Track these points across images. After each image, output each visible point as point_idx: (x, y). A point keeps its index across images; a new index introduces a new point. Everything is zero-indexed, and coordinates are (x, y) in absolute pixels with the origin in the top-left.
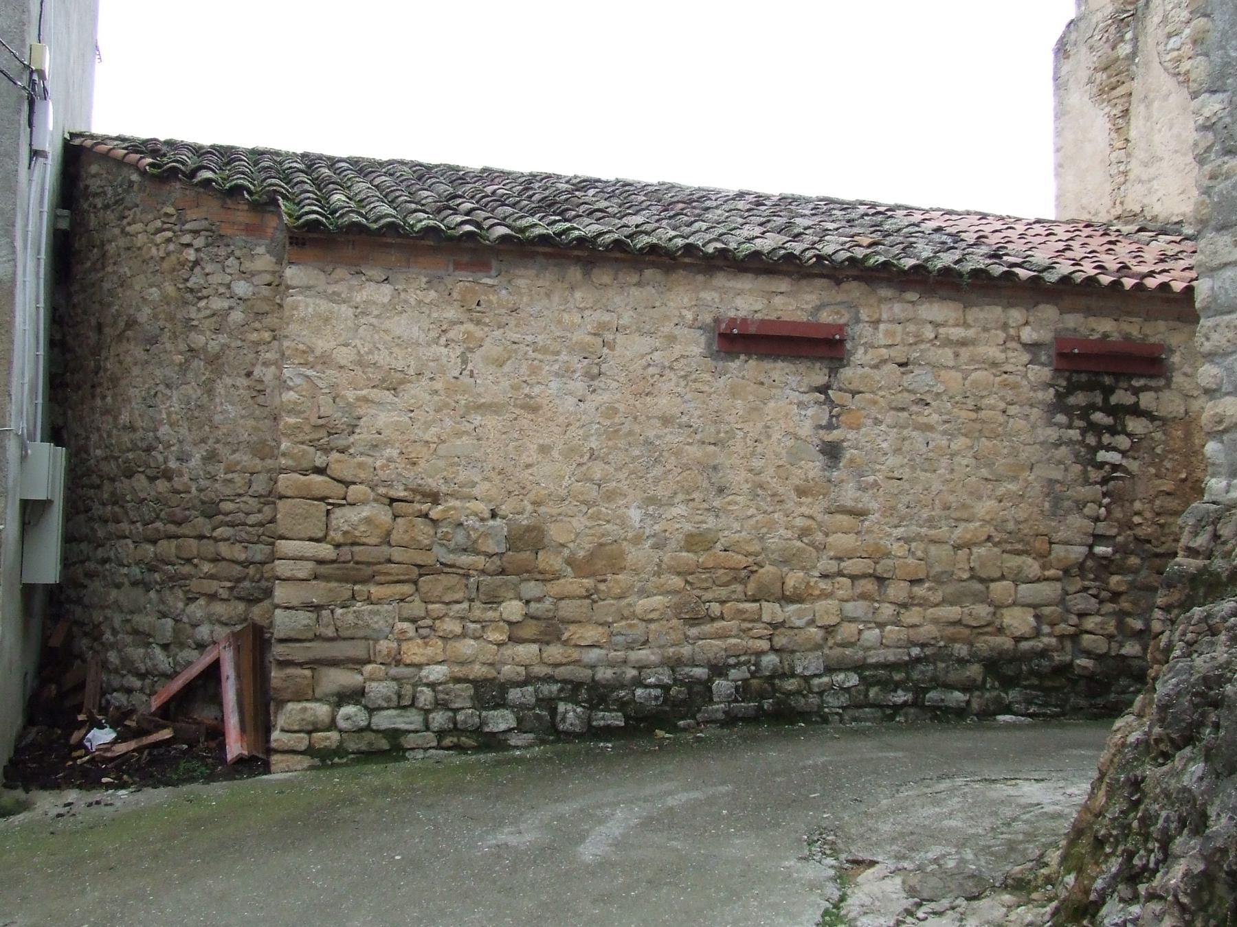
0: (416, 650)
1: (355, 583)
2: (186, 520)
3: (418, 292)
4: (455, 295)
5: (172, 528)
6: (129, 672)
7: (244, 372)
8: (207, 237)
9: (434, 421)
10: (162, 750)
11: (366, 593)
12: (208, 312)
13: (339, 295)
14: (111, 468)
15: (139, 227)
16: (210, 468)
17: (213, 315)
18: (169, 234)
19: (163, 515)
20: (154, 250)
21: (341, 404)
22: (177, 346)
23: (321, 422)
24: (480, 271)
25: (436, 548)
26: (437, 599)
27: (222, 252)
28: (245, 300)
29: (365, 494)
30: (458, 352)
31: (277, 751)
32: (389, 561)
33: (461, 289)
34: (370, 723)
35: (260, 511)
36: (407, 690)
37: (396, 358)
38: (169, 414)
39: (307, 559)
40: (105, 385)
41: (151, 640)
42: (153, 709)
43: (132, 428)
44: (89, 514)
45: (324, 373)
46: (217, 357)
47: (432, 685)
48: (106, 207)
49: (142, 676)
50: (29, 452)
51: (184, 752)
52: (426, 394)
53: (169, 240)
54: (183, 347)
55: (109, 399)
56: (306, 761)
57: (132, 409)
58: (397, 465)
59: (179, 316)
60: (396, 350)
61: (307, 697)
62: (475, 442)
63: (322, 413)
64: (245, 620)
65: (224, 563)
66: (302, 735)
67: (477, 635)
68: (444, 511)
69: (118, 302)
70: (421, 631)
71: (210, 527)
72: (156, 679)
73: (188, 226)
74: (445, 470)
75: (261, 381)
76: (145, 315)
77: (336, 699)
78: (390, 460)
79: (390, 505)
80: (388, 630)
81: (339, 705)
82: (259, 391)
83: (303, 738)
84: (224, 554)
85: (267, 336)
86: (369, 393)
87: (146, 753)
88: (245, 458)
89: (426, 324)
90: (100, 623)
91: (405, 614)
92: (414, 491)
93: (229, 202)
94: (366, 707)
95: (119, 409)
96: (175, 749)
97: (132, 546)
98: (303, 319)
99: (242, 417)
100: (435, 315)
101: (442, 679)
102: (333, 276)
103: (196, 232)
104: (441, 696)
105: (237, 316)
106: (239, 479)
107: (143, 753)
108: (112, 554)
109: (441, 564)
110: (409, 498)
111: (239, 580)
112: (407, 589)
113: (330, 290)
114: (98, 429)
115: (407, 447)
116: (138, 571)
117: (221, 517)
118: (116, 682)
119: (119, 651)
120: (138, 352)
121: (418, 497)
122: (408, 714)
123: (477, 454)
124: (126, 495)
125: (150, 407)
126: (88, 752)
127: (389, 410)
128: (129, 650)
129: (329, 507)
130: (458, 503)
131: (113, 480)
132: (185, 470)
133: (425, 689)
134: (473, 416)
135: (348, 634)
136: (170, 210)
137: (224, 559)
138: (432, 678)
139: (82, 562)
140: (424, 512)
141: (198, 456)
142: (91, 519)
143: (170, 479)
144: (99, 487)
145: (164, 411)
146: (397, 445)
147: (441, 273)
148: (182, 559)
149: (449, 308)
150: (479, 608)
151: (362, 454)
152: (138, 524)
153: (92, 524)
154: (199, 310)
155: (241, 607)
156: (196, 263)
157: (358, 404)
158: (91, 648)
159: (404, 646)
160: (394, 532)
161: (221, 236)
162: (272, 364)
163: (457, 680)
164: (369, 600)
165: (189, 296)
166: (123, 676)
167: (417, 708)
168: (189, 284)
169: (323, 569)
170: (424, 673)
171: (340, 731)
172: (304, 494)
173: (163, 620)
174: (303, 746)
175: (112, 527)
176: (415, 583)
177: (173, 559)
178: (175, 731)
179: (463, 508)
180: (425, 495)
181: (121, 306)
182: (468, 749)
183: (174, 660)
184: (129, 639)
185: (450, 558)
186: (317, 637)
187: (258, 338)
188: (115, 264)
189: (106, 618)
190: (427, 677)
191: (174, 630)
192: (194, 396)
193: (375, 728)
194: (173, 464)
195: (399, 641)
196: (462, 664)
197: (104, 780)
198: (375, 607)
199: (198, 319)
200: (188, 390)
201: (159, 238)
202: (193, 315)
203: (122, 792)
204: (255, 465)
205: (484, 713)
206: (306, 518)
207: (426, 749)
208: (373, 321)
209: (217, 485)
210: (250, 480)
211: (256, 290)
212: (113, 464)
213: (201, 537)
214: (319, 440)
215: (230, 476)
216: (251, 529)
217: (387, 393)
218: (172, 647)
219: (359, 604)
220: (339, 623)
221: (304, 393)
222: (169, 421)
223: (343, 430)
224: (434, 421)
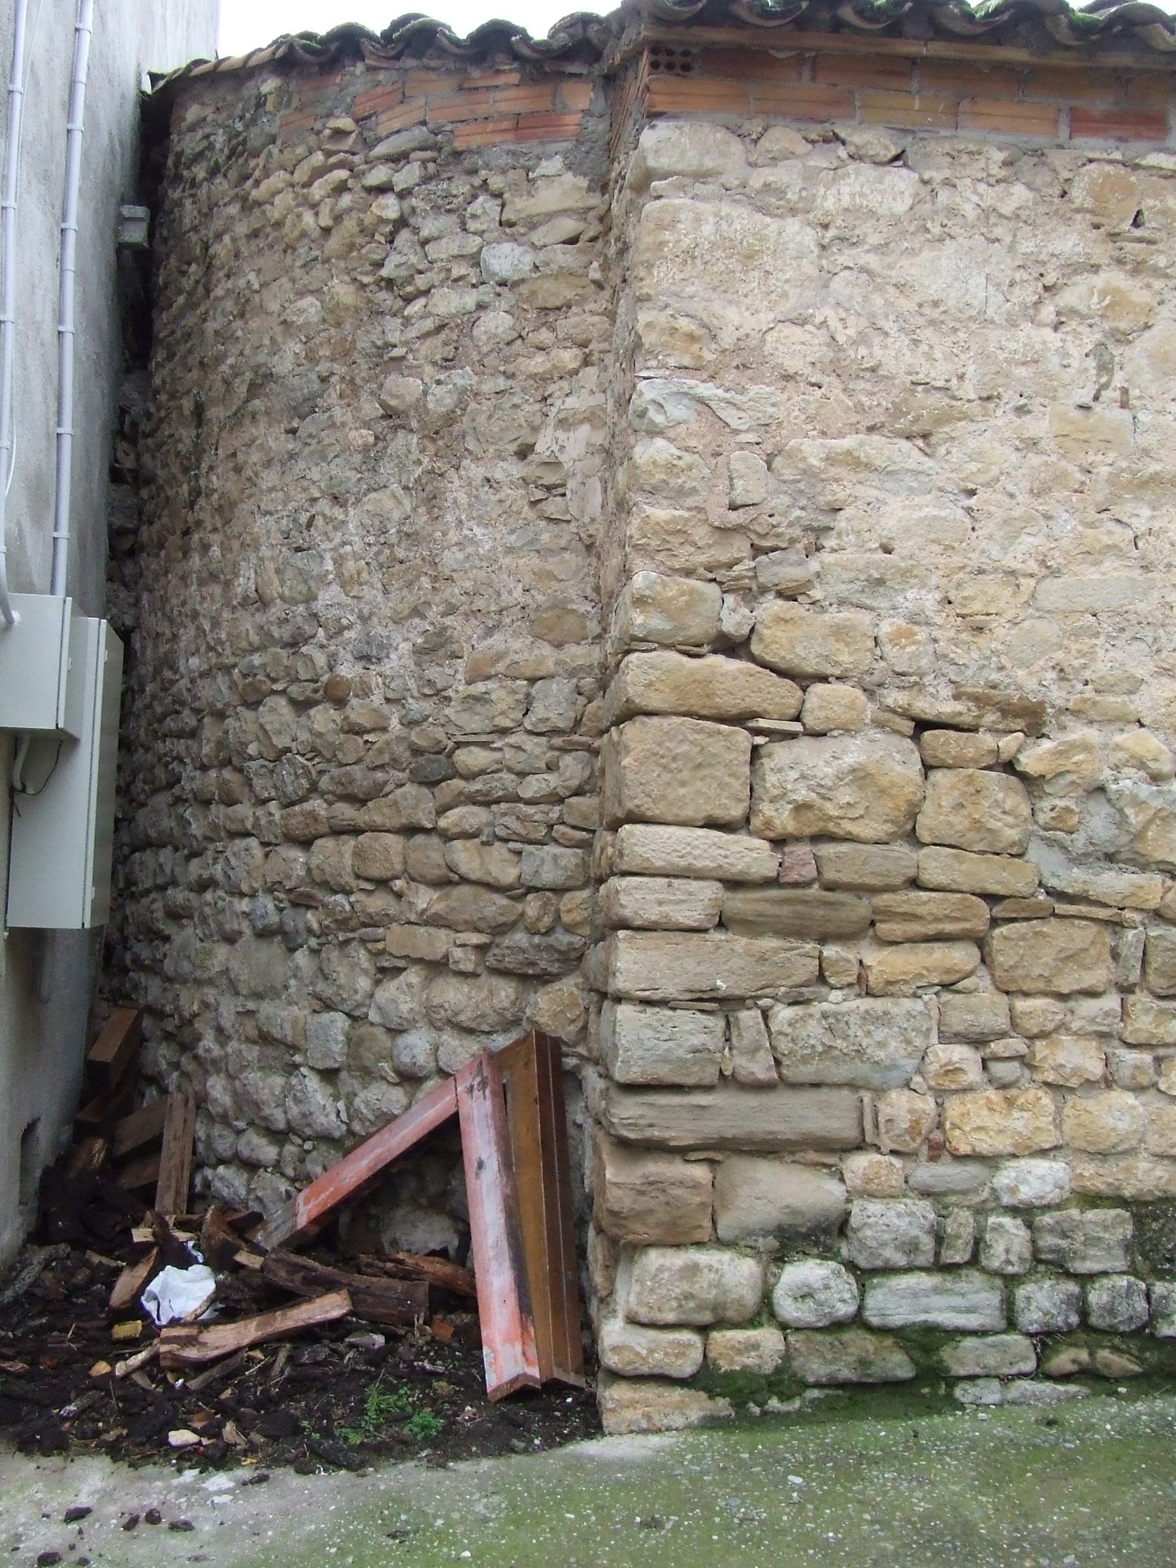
0: (983, 1117)
1: (823, 940)
2: (377, 792)
3: (982, 187)
4: (1078, 195)
5: (346, 812)
6: (251, 1124)
7: (513, 447)
8: (424, 163)
9: (1028, 520)
10: (323, 1353)
11: (855, 969)
12: (429, 324)
13: (780, 193)
14: (217, 691)
15: (278, 179)
16: (433, 673)
17: (440, 328)
18: (342, 174)
19: (324, 783)
20: (308, 218)
21: (788, 474)
22: (358, 409)
23: (735, 517)
24: (1139, 136)
25: (1036, 852)
26: (1041, 985)
27: (461, 187)
28: (516, 284)
29: (851, 707)
30: (1091, 339)
31: (616, 1376)
32: (915, 883)
33: (1093, 181)
34: (861, 1308)
35: (551, 768)
36: (961, 1223)
37: (930, 358)
38: (339, 561)
39: (699, 875)
40: (208, 525)
41: (298, 1058)
42: (302, 1221)
43: (261, 602)
44: (176, 790)
45: (743, 391)
46: (450, 419)
47: (1025, 1212)
48: (214, 172)
49: (279, 1136)
50: (16, 615)
51: (376, 1358)
52: (1008, 451)
53: (341, 188)
54: (371, 409)
55: (216, 551)
56: (697, 1406)
57: (261, 559)
58: (936, 633)
59: (363, 343)
60: (927, 334)
61: (699, 1235)
62: (1136, 574)
63: (740, 497)
64: (516, 1022)
65: (465, 889)
66: (686, 1336)
67: (1144, 1080)
68: (1059, 753)
69: (234, 350)
70: (997, 1068)
71: (431, 805)
72: (308, 1146)
73: (381, 149)
74: (1060, 646)
75: (553, 464)
76: (289, 356)
77: (772, 1242)
78: (916, 618)
79: (916, 737)
80: (910, 1064)
81: (780, 1258)
82: (549, 488)
83: (689, 1345)
84: (464, 869)
85: (569, 358)
86: (861, 444)
87: (282, 1356)
88: (517, 644)
89: (1003, 265)
90: (195, 1015)
91: (958, 1021)
92: (979, 700)
93: (476, 73)
94: (851, 1266)
95: (235, 565)
96: (352, 1346)
97: (258, 852)
98: (690, 255)
99: (510, 550)
100: (1027, 246)
101: (1053, 1196)
102: (764, 143)
103: (398, 159)
104: (1048, 1241)
105: (497, 322)
106: (502, 693)
107: (275, 1353)
108: (218, 871)
109: (1051, 892)
110: (967, 719)
111: (501, 930)
112: (962, 956)
113: (757, 180)
114: (195, 615)
115: (959, 586)
116: (271, 906)
117: (457, 784)
118: (224, 1144)
119: (231, 1077)
120: (276, 441)
121: (990, 718)
122: (962, 1286)
123: (1142, 607)
124: (246, 745)
125: (299, 549)
126: (151, 1331)
127: (911, 490)
128: (253, 1076)
129: (760, 740)
130: (1092, 734)
131: (221, 715)
132: (375, 681)
133: (1007, 1221)
134: (1129, 507)
135: (807, 1072)
136: (345, 123)
137: (464, 880)
138: (1025, 1194)
139: (163, 888)
140: (1005, 757)
141: (405, 647)
142: (179, 800)
143: (340, 703)
144: (193, 734)
145: (328, 556)
146: (934, 580)
147: (1039, 141)
148: (368, 880)
149: (1062, 229)
150: (1147, 1011)
151: (842, 602)
152: (273, 806)
153: (181, 810)
154: (407, 322)
155: (505, 992)
156: (401, 223)
157: (833, 471)
158: (177, 1066)
159: (954, 1108)
160: (928, 807)
161: (457, 154)
162: (582, 422)
163: (1091, 1200)
164: (863, 986)
165: (385, 298)
166: (239, 1132)
167: (984, 1270)
168: (384, 272)
169: (740, 903)
170: (1004, 1178)
171: (784, 1327)
172: (694, 703)
173: (326, 1017)
174: (687, 1367)
175: (218, 812)
176: (981, 942)
177: (349, 880)
178: (354, 1295)
179: (1105, 746)
180: (1006, 710)
181: (241, 354)
182: (1118, 1381)
183: (349, 1105)
184: (252, 1053)
185: (1072, 879)
186: (728, 1081)
187: (548, 365)
188: (228, 276)
189: (206, 1005)
190: (1013, 1191)
191: (349, 1039)
192: (396, 515)
193: (875, 1321)
194: (348, 670)
195: (940, 1094)
196: (1103, 1155)
197: (180, 1437)
198: (878, 1005)
199: (406, 343)
200: (384, 501)
201: (318, 190)
202: (393, 338)
203: (220, 1481)
204: (540, 661)
205: (1160, 1288)
206: (699, 766)
207: (1006, 1380)
208: (873, 261)
209: (447, 711)
210: (528, 695)
211: (541, 256)
212: (222, 681)
213: (411, 830)
214: (730, 566)
215: (480, 687)
216: (530, 810)
217: (905, 445)
218: (344, 1075)
219: (836, 995)
220: (784, 1045)
221: (692, 443)
222: (340, 575)
223: (792, 541)
224: (1028, 520)
